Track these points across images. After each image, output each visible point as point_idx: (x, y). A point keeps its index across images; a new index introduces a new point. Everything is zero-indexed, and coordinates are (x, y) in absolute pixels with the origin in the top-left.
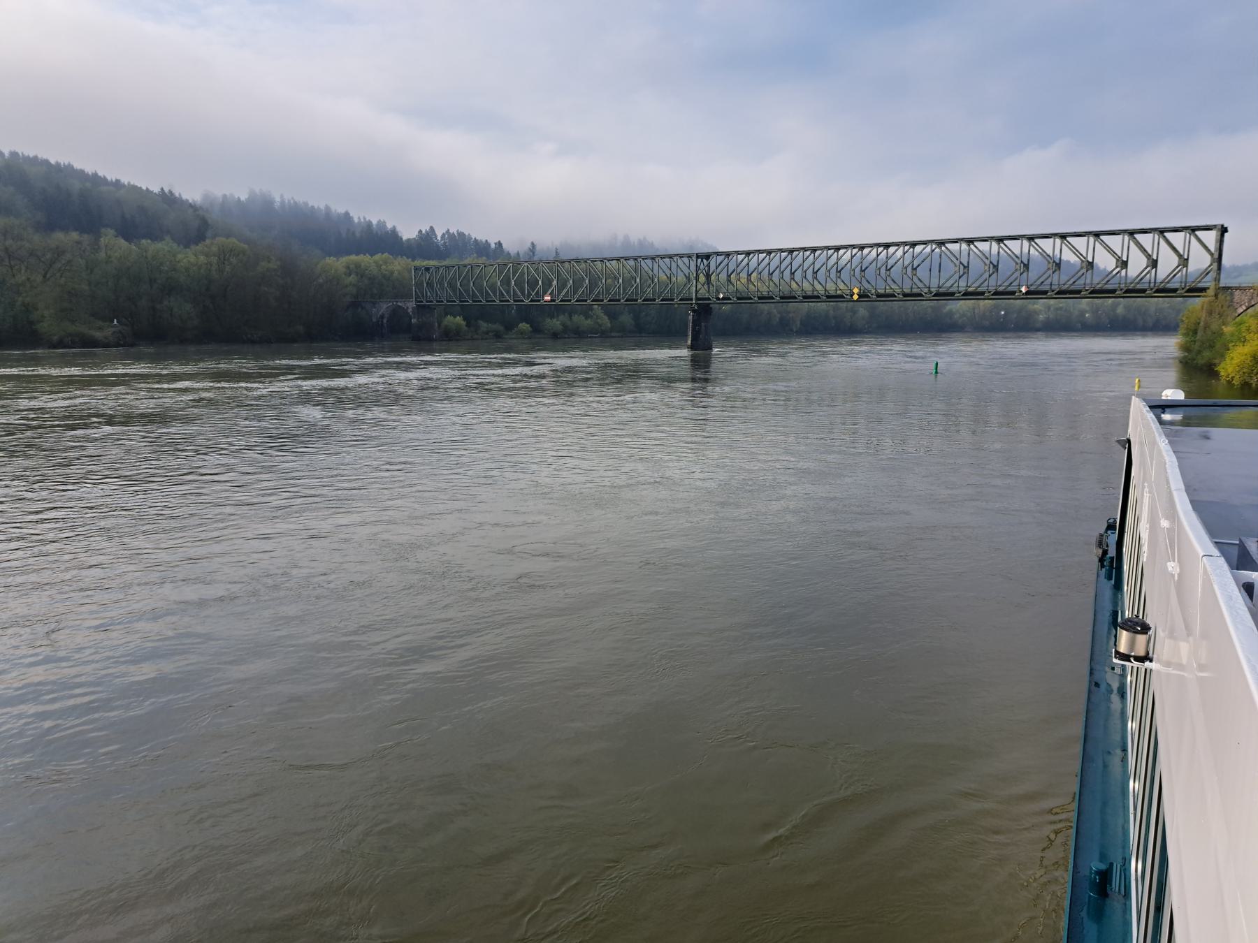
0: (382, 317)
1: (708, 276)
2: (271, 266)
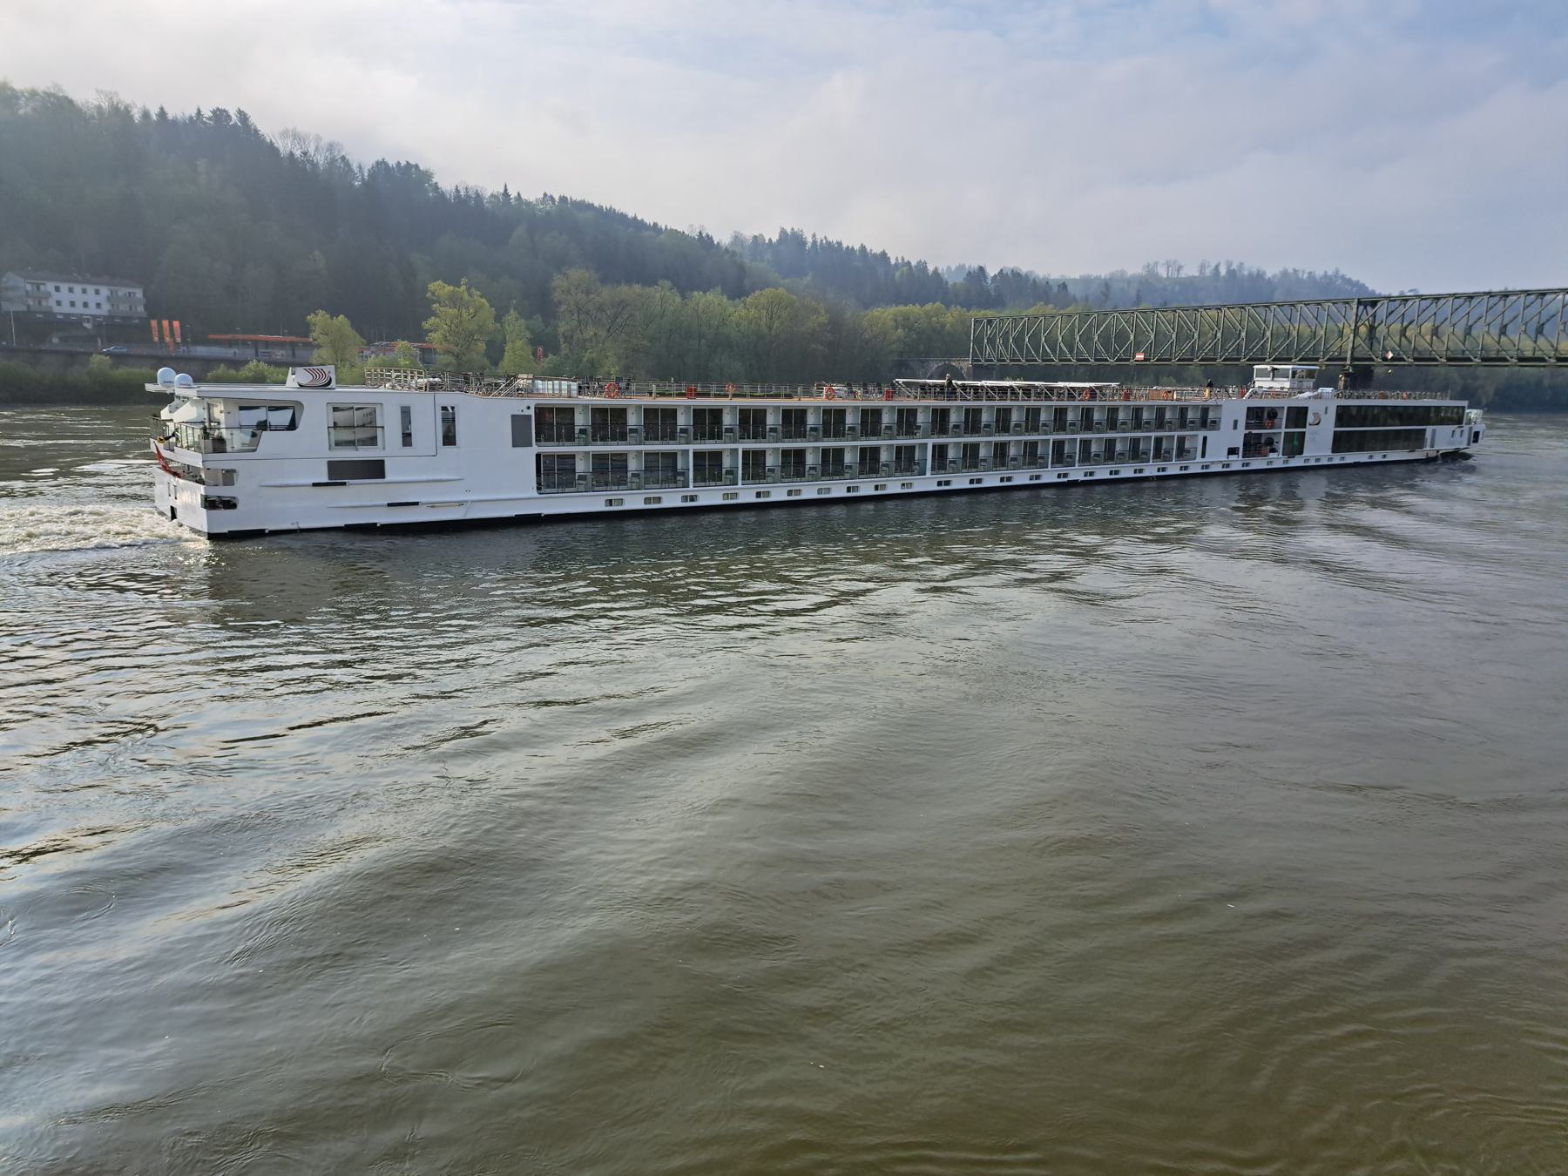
1: (1372, 329)
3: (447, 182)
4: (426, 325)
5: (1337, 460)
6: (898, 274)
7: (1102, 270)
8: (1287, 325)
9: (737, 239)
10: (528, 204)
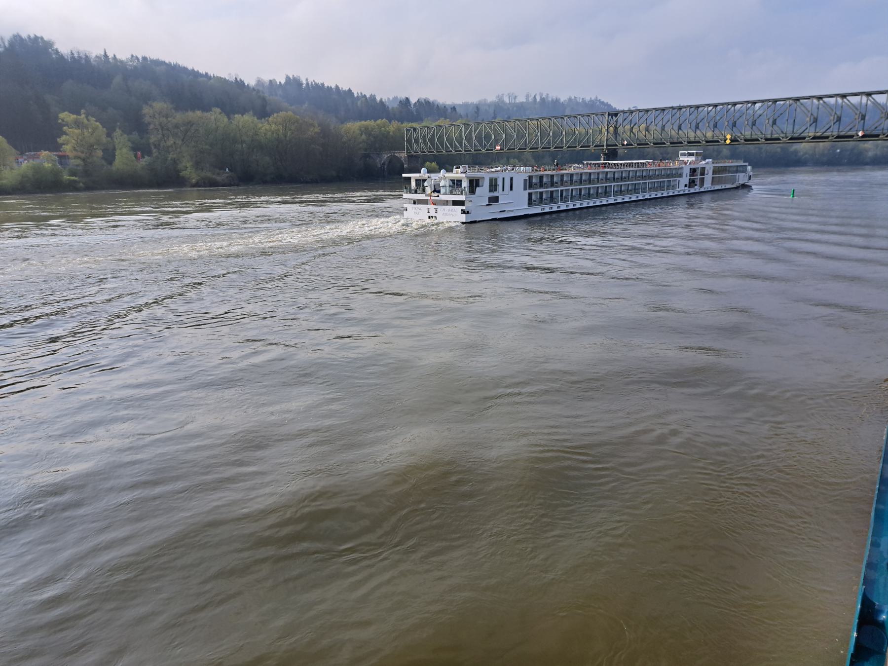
0: (384, 164)
1: (616, 128)
2: (317, 130)
3: (64, 47)
4: (60, 140)
6: (359, 103)
10: (121, 62)
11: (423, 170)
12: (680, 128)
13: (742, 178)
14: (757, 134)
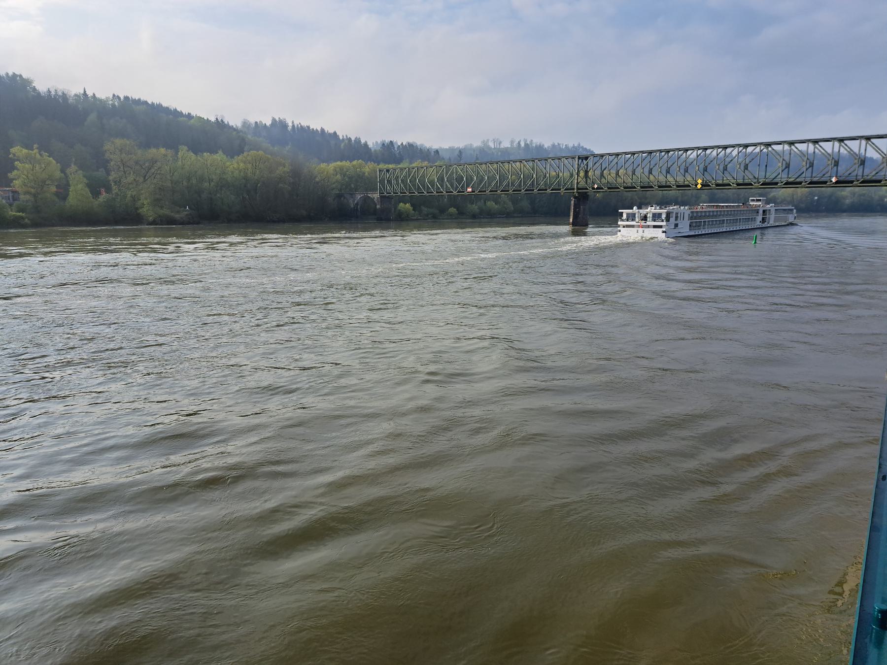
0: (357, 204)
1: (586, 172)
3: (42, 86)
4: (10, 176)
5: (692, 233)
6: (342, 145)
7: (460, 144)
8: (544, 171)
9: (245, 123)
10: (100, 100)
11: (635, 208)
12: (650, 172)
13: (791, 218)
14: (728, 179)
